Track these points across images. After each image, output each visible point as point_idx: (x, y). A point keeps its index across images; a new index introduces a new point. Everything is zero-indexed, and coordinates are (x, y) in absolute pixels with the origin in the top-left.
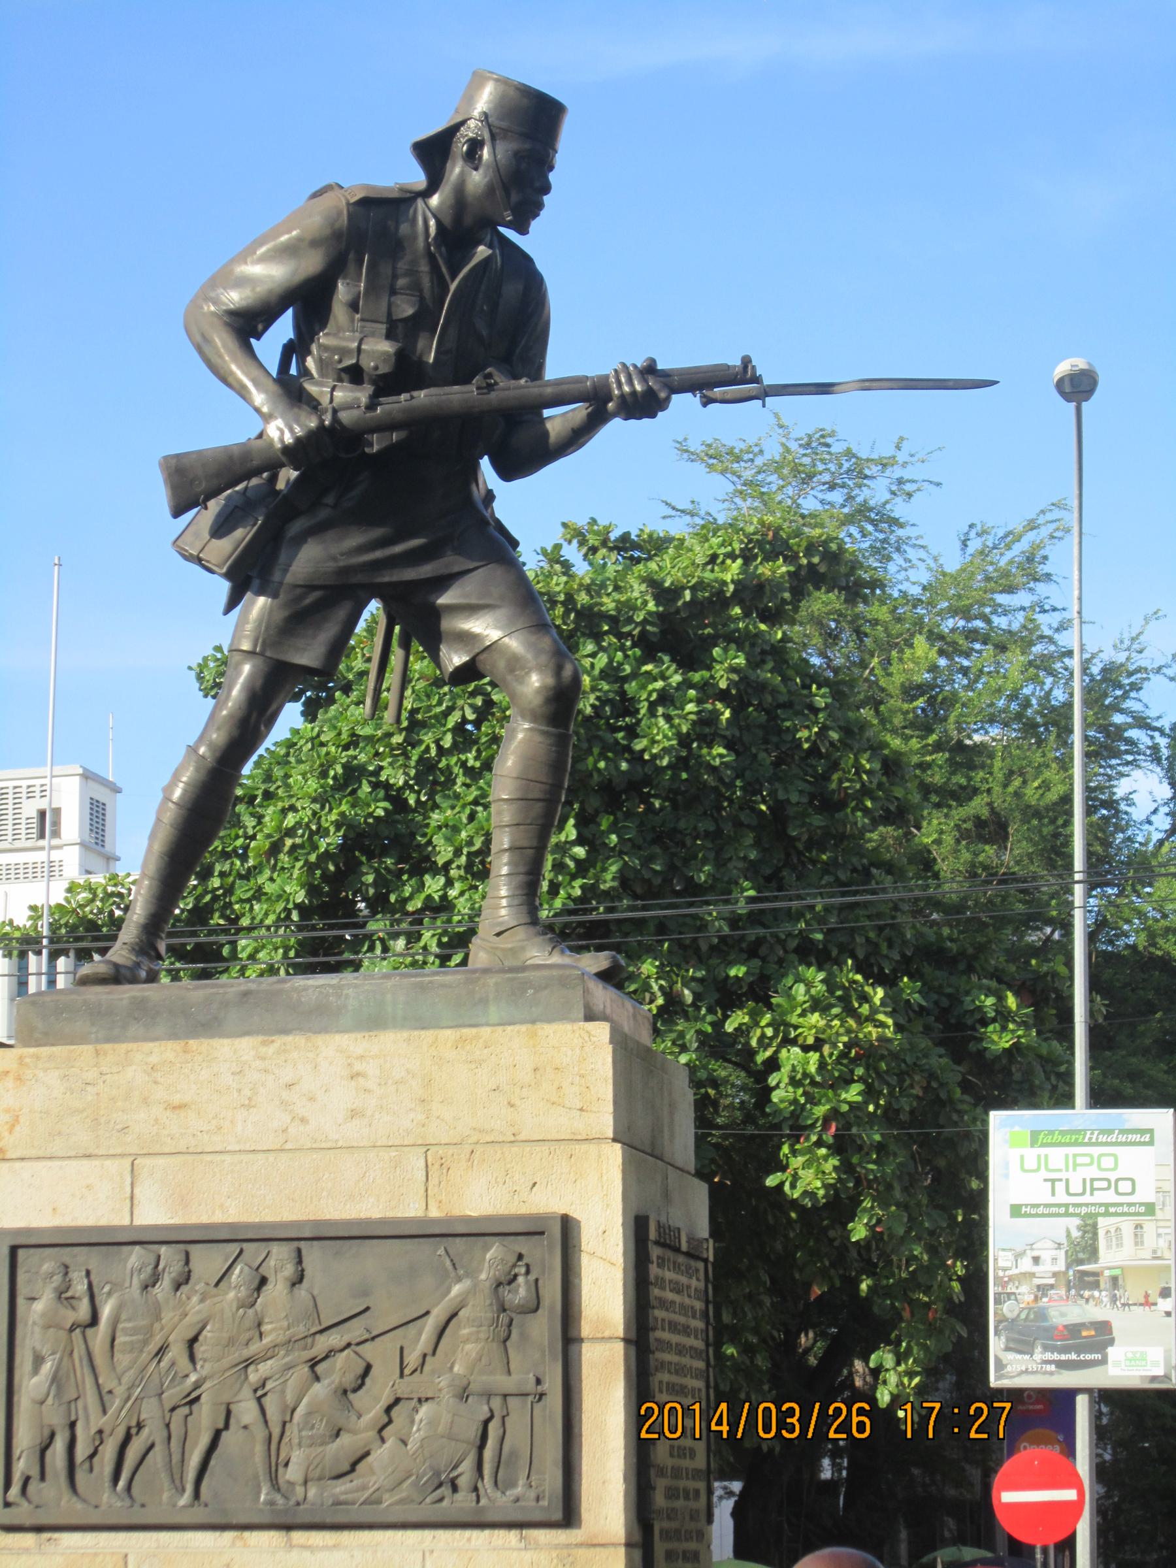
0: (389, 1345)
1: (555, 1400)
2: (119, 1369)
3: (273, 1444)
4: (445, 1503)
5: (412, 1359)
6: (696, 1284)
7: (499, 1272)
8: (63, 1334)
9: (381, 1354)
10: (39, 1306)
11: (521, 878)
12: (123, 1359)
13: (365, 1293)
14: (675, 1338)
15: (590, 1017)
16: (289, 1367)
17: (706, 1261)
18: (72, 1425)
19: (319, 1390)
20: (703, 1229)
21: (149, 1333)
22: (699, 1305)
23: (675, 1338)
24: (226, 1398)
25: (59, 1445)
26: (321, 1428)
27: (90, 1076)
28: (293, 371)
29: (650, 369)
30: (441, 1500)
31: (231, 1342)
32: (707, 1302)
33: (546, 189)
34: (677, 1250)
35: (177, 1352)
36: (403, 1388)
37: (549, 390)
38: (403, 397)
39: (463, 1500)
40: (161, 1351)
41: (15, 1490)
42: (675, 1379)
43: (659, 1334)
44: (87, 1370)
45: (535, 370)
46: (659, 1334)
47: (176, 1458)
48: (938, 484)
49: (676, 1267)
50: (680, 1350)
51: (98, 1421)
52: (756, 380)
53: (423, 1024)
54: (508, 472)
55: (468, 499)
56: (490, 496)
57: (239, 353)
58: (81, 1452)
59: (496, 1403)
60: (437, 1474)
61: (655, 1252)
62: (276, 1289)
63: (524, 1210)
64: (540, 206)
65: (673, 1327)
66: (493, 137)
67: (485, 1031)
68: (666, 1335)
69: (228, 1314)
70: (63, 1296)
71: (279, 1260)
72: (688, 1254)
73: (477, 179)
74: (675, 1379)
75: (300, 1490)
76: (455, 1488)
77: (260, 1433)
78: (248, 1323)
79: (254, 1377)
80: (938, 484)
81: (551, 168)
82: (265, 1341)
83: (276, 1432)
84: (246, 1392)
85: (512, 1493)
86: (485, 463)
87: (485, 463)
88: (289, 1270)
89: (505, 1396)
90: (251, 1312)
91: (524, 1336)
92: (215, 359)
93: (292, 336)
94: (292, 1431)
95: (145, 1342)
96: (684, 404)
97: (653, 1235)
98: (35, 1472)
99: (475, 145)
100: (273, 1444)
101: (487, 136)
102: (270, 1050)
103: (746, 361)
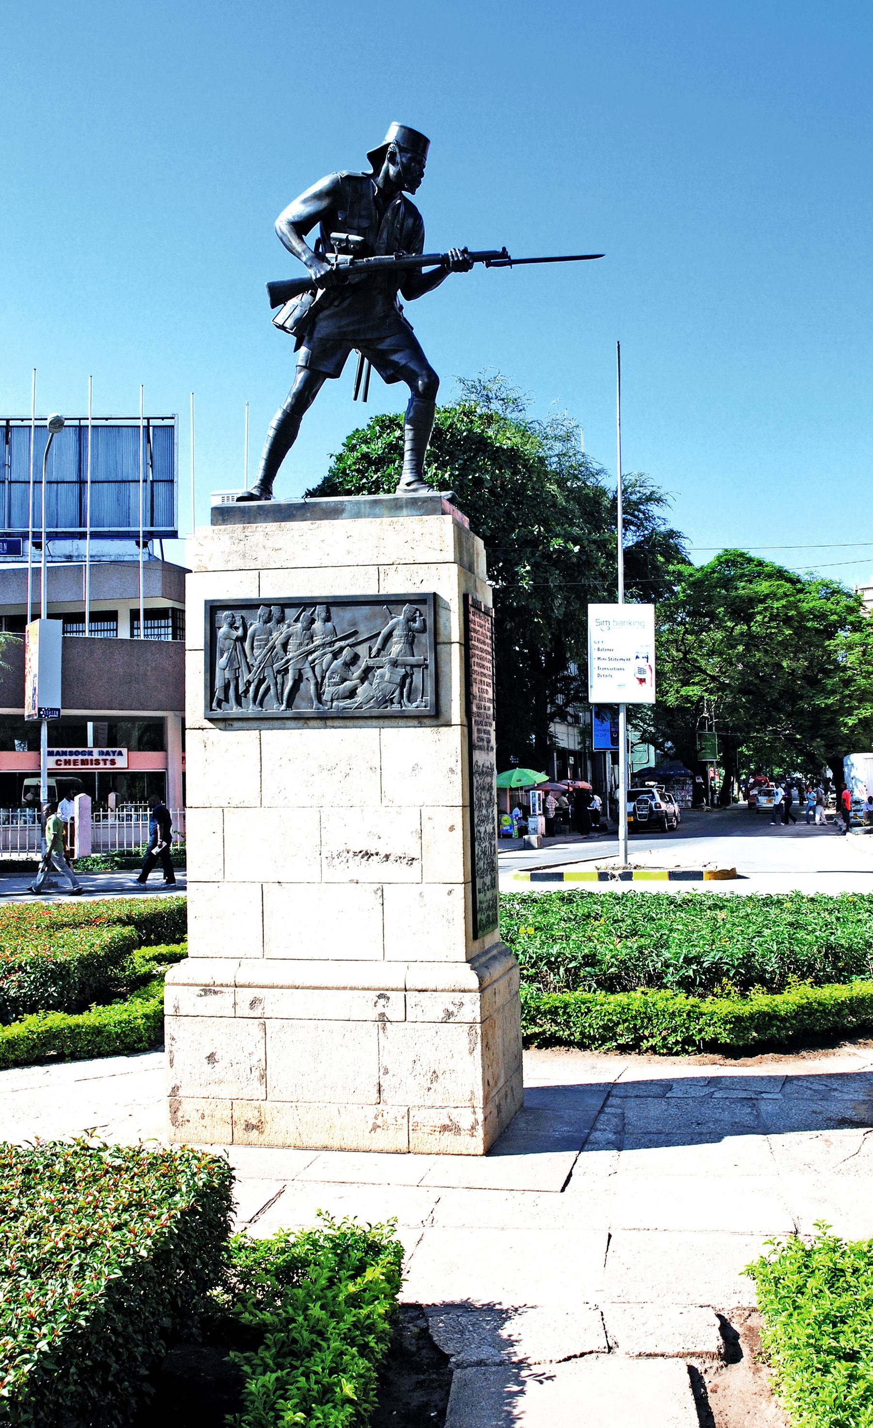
0: (366, 646)
1: (432, 667)
2: (256, 655)
3: (319, 686)
4: (388, 708)
5: (374, 650)
6: (488, 625)
7: (408, 615)
8: (232, 642)
9: (362, 650)
10: (222, 630)
11: (414, 462)
12: (257, 652)
13: (354, 625)
14: (480, 645)
15: (444, 513)
16: (324, 654)
17: (491, 617)
18: (237, 679)
19: (339, 662)
20: (490, 604)
21: (267, 640)
22: (489, 634)
23: (480, 645)
24: (299, 667)
25: (232, 687)
26: (337, 679)
27: (242, 537)
28: (320, 250)
29: (465, 251)
30: (386, 707)
31: (301, 644)
32: (492, 633)
33: (422, 175)
34: (480, 610)
35: (278, 648)
36: (371, 663)
37: (424, 259)
38: (365, 260)
39: (396, 707)
40: (273, 648)
41: (214, 704)
42: (479, 661)
43: (473, 642)
44: (242, 656)
45: (420, 250)
46: (473, 642)
47: (279, 691)
48: (610, 1236)
49: (480, 617)
50: (482, 650)
51: (247, 677)
52: (509, 257)
53: (376, 516)
54: (410, 295)
55: (393, 307)
56: (401, 308)
57: (298, 241)
58: (241, 688)
59: (408, 668)
60: (385, 696)
61: (472, 609)
62: (318, 625)
63: (418, 591)
64: (420, 182)
65: (479, 640)
66: (400, 151)
67: (401, 519)
68: (476, 643)
69: (299, 634)
70: (232, 626)
71: (320, 610)
72: (484, 613)
73: (392, 170)
74: (479, 661)
75: (329, 704)
76: (392, 703)
77: (312, 682)
78: (306, 637)
79: (310, 658)
80: (610, 1236)
81: (424, 167)
82: (315, 644)
83: (319, 680)
84: (307, 665)
85: (415, 705)
86: (399, 292)
87: (399, 292)
88: (323, 615)
89: (409, 1152)
90: (308, 632)
91: (419, 642)
92: (287, 243)
93: (319, 236)
94: (326, 681)
95: (266, 645)
96: (479, 266)
97: (470, 602)
98: (222, 697)
99: (393, 154)
100: (319, 686)
101: (397, 151)
102: (315, 526)
103: (504, 249)
